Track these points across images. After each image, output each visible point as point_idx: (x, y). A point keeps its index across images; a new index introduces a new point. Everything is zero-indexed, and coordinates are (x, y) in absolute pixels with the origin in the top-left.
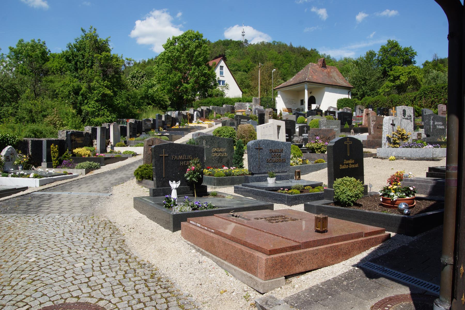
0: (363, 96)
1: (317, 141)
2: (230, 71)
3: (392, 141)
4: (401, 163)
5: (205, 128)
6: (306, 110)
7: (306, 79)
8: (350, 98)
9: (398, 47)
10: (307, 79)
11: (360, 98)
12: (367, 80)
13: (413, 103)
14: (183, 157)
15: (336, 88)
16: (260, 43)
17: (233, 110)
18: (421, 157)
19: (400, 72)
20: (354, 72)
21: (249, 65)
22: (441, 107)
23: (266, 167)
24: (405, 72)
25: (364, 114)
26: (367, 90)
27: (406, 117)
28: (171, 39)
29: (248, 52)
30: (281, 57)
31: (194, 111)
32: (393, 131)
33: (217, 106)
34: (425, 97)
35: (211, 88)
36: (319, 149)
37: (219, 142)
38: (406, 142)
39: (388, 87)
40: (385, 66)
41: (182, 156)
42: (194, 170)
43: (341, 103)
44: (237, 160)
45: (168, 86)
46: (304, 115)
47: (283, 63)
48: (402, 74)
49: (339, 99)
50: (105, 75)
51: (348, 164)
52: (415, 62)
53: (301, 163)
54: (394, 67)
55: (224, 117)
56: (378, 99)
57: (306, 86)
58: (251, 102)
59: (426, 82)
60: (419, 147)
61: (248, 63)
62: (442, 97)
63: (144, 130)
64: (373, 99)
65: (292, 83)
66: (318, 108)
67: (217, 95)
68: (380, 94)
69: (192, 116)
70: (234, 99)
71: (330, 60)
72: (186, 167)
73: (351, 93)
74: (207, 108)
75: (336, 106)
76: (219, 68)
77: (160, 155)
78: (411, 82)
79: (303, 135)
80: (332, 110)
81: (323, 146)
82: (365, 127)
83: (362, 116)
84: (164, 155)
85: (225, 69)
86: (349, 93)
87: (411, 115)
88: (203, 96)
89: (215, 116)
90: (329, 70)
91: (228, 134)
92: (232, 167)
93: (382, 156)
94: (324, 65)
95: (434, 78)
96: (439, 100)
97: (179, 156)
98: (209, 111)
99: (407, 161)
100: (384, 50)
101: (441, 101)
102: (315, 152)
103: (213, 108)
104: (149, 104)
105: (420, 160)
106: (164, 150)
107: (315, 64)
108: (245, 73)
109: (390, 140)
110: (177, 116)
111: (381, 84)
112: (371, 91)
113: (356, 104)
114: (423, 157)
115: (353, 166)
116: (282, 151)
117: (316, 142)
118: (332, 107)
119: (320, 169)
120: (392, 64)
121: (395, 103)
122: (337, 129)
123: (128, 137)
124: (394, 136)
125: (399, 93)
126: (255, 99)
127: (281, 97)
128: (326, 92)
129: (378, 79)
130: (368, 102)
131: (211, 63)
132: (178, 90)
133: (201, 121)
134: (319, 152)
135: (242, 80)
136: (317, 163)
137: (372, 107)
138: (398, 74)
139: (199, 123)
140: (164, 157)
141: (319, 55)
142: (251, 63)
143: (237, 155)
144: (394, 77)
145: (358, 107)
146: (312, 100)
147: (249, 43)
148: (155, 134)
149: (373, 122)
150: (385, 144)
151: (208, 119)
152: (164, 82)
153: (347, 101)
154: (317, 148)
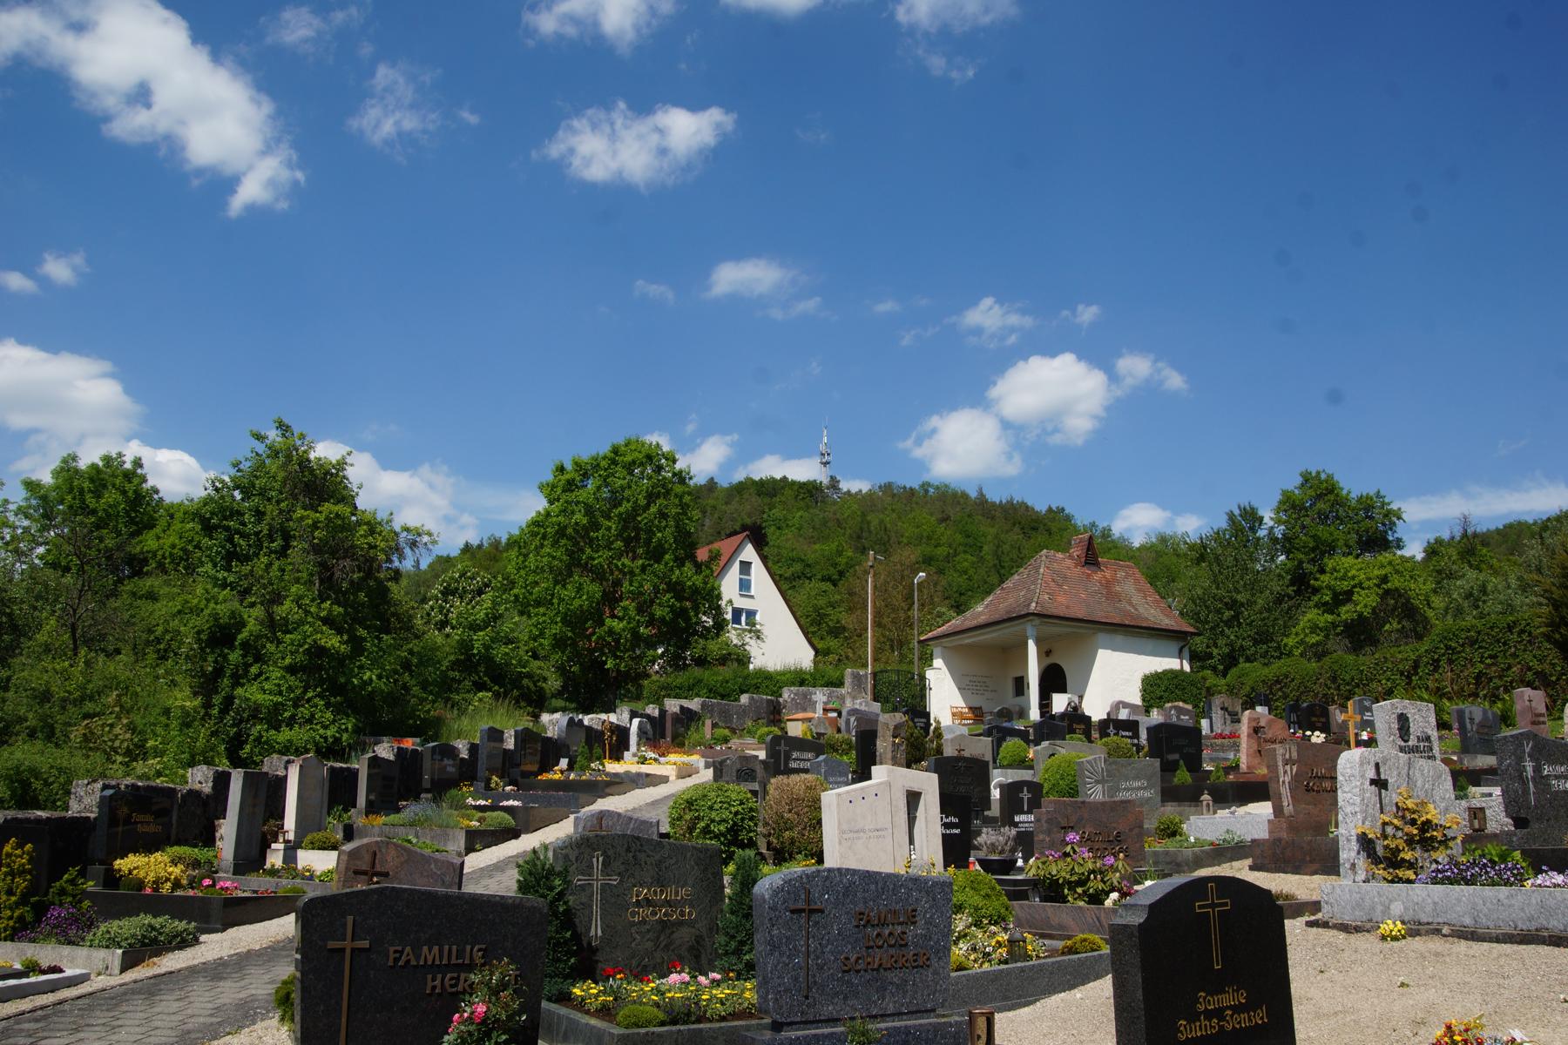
0: (1231, 661)
1: (1068, 849)
2: (777, 580)
3: (1380, 851)
4: (1437, 954)
5: (664, 780)
6: (1035, 714)
7: (1029, 605)
8: (1187, 668)
9: (1337, 495)
10: (1034, 605)
11: (1221, 667)
12: (1242, 605)
13: (1409, 683)
14: (441, 951)
15: (1140, 635)
16: (880, 487)
17: (775, 714)
18: (1520, 926)
19: (1353, 578)
20: (1200, 579)
21: (842, 560)
22: (1526, 698)
23: (837, 994)
24: (1369, 579)
25: (1244, 728)
26: (1244, 639)
27: (1410, 743)
28: (569, 466)
29: (838, 516)
30: (949, 533)
31: (633, 715)
32: (1382, 812)
33: (723, 697)
34: (1450, 662)
35: (706, 634)
36: (1082, 882)
37: (659, 863)
38: (1441, 856)
39: (1315, 628)
40: (1301, 556)
41: (436, 948)
42: (484, 1022)
43: (1156, 689)
44: (733, 937)
45: (553, 626)
46: (1023, 735)
47: (955, 555)
48: (1360, 585)
49: (1147, 672)
50: (328, 585)
51: (1218, 1013)
52: (1399, 544)
53: (1003, 951)
54: (1330, 563)
55: (741, 737)
56: (1284, 670)
57: (1030, 629)
58: (840, 684)
59: (1447, 609)
60: (1507, 883)
61: (840, 553)
62: (1511, 661)
63: (426, 784)
64: (1266, 671)
65: (982, 619)
66: (1076, 709)
67: (723, 660)
68: (1290, 654)
69: (622, 733)
70: (783, 673)
71: (1113, 541)
72: (452, 1002)
73: (1190, 651)
74: (682, 707)
75: (1137, 700)
76: (736, 567)
77: (332, 944)
78: (1395, 609)
79: (1017, 819)
80: (1123, 715)
81: (1093, 872)
82: (1251, 778)
83: (1234, 735)
84: (347, 944)
85: (759, 573)
86: (1181, 651)
87: (1430, 732)
88: (676, 662)
89: (709, 736)
90: (1108, 574)
91: (726, 814)
92: (706, 975)
93: (1347, 919)
94: (1091, 557)
95: (1471, 594)
96: (1503, 670)
97: (425, 948)
98: (688, 718)
99: (1462, 946)
100: (1290, 506)
101: (1510, 672)
102: (1064, 900)
103: (703, 705)
104: (480, 687)
105: (1521, 942)
106: (350, 919)
107: (1060, 555)
108: (827, 586)
109: (1374, 848)
110: (564, 735)
111: (1290, 618)
112: (1256, 642)
113: (1210, 692)
114: (1533, 926)
115: (1244, 1021)
116: (912, 918)
117: (1066, 855)
118: (1126, 705)
119: (1084, 980)
120: (1324, 549)
121: (1348, 684)
122: (1147, 794)
123: (360, 812)
124: (1389, 830)
125: (1356, 648)
126: (853, 674)
127: (945, 669)
128: (1100, 651)
129: (1279, 600)
130: (1249, 683)
131: (702, 554)
132: (589, 638)
133: (653, 756)
134: (1080, 897)
135: (817, 609)
136: (1071, 950)
137: (1266, 702)
138: (1345, 585)
139: (643, 761)
140: (348, 952)
141: (1075, 526)
142: (850, 554)
143: (733, 918)
144: (1335, 595)
145: (1217, 701)
146: (1053, 680)
147: (845, 490)
148: (470, 801)
149: (1288, 767)
150: (1353, 865)
151: (682, 745)
152: (542, 610)
153: (1175, 681)
154: (1069, 883)
